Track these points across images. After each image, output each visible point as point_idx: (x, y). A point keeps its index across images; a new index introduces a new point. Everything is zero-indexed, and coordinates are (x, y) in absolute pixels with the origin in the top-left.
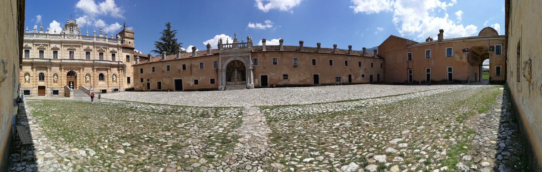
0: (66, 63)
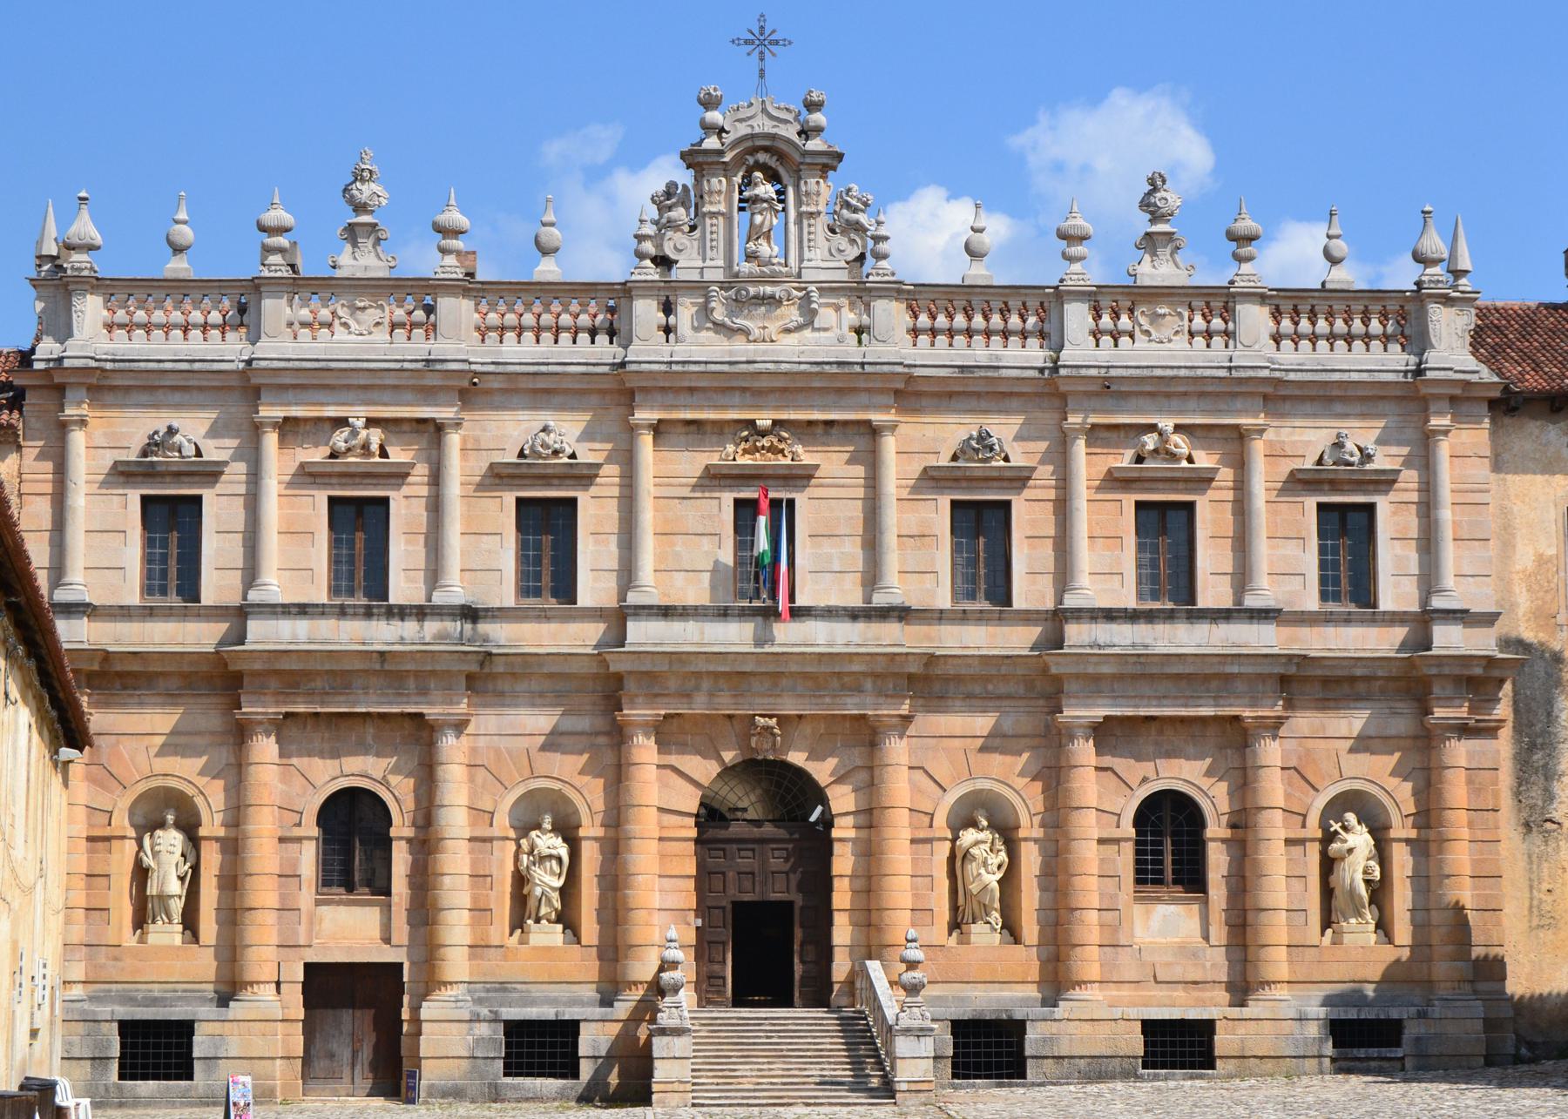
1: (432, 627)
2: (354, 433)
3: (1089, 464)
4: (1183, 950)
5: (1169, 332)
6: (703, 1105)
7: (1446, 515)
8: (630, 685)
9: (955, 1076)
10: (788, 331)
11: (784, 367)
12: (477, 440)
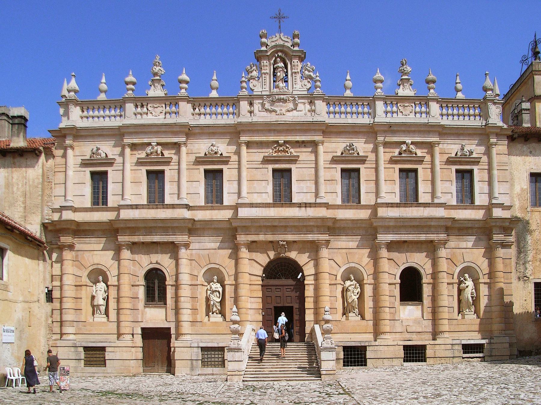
0: (211, 222)
2: (153, 148)
3: (384, 156)
4: (416, 321)
5: (409, 112)
6: (247, 381)
7: (495, 172)
8: (239, 230)
9: (344, 366)
10: (289, 111)
12: (191, 150)
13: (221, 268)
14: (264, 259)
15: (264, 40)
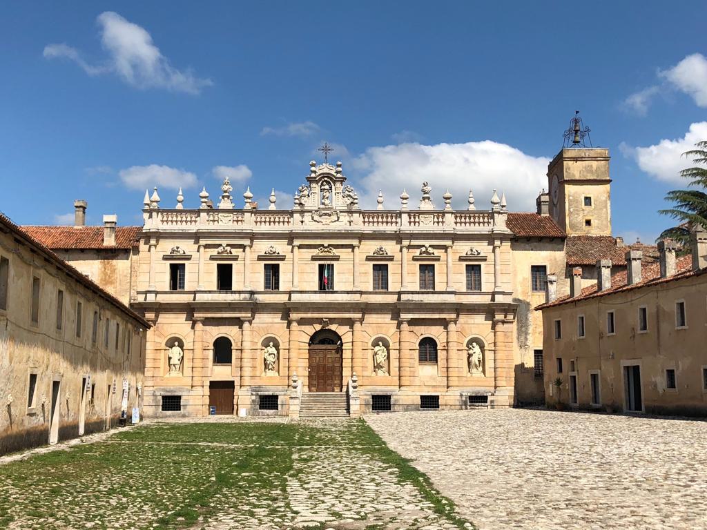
1: (243, 296)
3: (408, 255)
4: (433, 378)
11: (331, 231)
13: (276, 337)
14: (311, 330)
15: (313, 169)
